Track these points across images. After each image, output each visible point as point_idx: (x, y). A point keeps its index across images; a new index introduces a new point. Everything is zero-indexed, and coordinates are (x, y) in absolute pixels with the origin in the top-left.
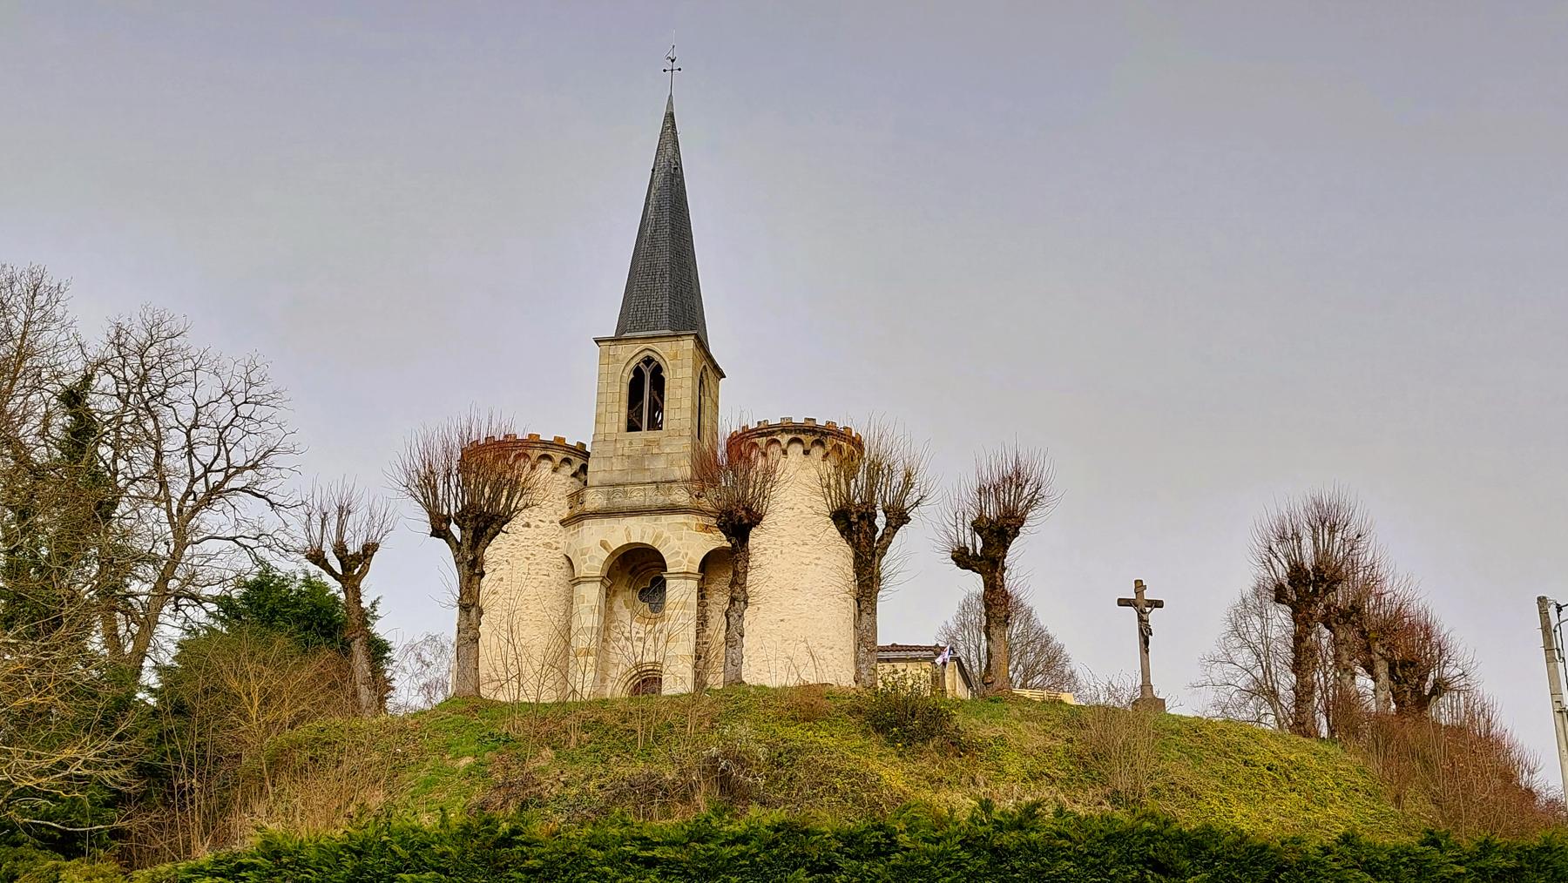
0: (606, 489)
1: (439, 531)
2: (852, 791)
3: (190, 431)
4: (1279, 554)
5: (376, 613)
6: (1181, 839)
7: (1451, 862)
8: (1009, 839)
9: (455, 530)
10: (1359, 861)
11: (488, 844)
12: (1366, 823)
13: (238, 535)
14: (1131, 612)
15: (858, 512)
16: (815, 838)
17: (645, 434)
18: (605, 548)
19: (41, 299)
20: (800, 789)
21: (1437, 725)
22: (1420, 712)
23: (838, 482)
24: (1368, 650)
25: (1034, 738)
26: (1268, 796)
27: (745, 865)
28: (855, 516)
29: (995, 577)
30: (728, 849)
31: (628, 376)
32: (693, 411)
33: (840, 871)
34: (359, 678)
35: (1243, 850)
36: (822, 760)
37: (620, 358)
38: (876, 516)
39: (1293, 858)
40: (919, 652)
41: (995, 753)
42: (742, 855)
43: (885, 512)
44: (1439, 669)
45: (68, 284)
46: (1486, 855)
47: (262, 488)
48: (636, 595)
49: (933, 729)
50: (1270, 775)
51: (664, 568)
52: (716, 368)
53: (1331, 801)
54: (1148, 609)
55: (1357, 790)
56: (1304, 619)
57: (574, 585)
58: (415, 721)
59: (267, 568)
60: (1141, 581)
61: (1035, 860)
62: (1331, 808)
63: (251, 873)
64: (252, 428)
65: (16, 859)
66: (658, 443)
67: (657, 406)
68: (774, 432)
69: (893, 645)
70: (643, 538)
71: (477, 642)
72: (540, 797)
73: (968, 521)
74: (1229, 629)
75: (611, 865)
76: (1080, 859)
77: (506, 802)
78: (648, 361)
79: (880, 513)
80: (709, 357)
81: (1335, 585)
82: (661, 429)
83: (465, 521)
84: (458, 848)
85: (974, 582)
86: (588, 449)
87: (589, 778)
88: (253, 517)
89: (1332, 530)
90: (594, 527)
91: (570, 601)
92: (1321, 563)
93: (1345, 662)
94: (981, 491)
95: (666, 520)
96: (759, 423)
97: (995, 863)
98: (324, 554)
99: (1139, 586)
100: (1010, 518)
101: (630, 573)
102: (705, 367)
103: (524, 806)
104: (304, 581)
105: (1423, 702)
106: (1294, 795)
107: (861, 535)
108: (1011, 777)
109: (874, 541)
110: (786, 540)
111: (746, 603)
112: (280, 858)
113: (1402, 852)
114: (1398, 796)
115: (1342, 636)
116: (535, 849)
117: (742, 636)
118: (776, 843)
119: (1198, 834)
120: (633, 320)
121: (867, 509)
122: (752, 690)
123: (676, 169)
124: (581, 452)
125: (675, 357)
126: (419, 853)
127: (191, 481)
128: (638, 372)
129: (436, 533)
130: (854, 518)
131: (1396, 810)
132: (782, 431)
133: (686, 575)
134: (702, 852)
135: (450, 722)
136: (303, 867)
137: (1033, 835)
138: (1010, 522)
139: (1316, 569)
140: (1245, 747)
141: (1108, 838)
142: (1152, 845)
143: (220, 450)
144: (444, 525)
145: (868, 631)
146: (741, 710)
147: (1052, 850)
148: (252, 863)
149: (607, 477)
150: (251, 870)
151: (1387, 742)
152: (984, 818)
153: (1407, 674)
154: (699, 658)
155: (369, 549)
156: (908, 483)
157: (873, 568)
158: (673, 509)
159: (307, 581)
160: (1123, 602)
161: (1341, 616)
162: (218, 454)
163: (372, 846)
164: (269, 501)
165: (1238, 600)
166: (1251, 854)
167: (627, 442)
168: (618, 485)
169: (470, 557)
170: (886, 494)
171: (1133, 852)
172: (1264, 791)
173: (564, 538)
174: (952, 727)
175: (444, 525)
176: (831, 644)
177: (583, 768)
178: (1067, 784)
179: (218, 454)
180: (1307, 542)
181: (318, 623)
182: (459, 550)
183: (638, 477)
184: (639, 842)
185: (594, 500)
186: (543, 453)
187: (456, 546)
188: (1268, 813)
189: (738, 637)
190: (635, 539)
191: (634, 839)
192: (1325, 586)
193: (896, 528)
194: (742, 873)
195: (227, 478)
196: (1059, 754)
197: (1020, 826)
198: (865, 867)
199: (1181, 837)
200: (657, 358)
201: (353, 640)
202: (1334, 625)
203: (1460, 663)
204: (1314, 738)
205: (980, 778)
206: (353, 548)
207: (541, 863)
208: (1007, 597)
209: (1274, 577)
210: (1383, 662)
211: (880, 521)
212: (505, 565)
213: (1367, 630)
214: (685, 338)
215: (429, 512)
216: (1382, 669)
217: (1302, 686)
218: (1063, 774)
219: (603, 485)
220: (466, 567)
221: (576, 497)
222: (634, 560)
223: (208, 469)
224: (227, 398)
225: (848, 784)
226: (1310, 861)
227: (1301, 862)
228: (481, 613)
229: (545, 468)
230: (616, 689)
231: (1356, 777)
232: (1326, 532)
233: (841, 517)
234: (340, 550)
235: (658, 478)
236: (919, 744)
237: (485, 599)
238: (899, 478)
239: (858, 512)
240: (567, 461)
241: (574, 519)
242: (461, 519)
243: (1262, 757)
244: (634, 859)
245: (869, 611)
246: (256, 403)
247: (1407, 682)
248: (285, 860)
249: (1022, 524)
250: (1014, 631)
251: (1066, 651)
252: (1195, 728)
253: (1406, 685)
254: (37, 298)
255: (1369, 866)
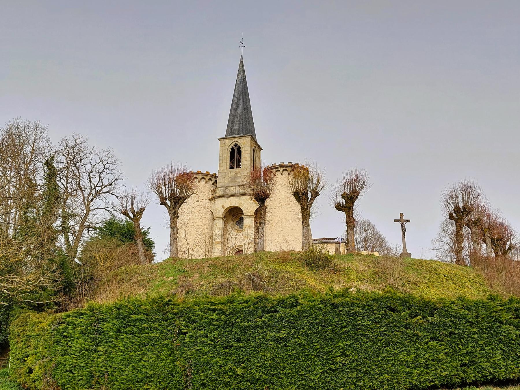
0: (223, 188)
1: (163, 203)
2: (296, 286)
3: (90, 174)
4: (450, 203)
5: (149, 232)
6: (400, 299)
7: (498, 306)
8: (338, 301)
9: (168, 202)
10: (464, 306)
11: (161, 305)
12: (479, 294)
13: (106, 207)
14: (399, 224)
15: (301, 192)
16: (269, 301)
17: (235, 170)
18: (223, 208)
19: (38, 132)
20: (279, 285)
21: (511, 261)
22: (504, 256)
23: (295, 183)
24: (484, 235)
25: (362, 267)
26: (444, 285)
27: (246, 311)
28: (301, 194)
29: (350, 213)
30: (240, 305)
31: (230, 150)
32: (251, 161)
33: (279, 312)
34: (140, 252)
35: (422, 303)
36: (287, 275)
37: (227, 145)
38: (308, 194)
39: (440, 305)
40: (332, 240)
41: (347, 272)
42: (245, 307)
43: (311, 192)
44: (511, 241)
45: (47, 127)
46: (511, 303)
47: (113, 192)
48: (235, 223)
49: (326, 264)
50: (445, 278)
51: (243, 214)
52: (259, 146)
53: (466, 287)
54: (405, 223)
55: (476, 283)
56: (459, 225)
57: (213, 220)
58: (156, 266)
59: (113, 216)
60: (402, 213)
61: (347, 308)
62: (466, 289)
63: (85, 316)
64: (109, 172)
65: (21, 313)
66: (239, 172)
67: (239, 161)
68: (278, 167)
69: (323, 238)
70: (235, 204)
71: (177, 239)
72: (193, 290)
73: (340, 194)
74: (441, 230)
75: (201, 311)
76: (363, 307)
77: (182, 292)
78: (236, 145)
79: (309, 193)
80: (256, 143)
81: (470, 213)
82: (241, 168)
83: (171, 199)
84: (151, 306)
85: (343, 215)
86: (217, 175)
87: (210, 283)
88: (111, 201)
89: (469, 194)
90: (220, 201)
91: (212, 225)
92: (465, 205)
93: (475, 239)
94: (345, 184)
95: (243, 198)
96: (273, 165)
97: (333, 309)
98: (127, 212)
99: (402, 215)
100: (354, 193)
101: (233, 216)
102: (255, 146)
103: (187, 293)
104: (125, 221)
105: (505, 253)
106: (453, 285)
107: (303, 200)
108: (352, 280)
109: (307, 202)
110: (283, 204)
111: (265, 224)
112: (93, 311)
113: (480, 303)
114: (491, 285)
115: (474, 230)
116: (176, 306)
117: (264, 235)
118: (257, 303)
119: (405, 298)
120: (231, 132)
121: (305, 191)
122: (266, 253)
123: (244, 80)
124: (215, 176)
125: (245, 143)
126: (138, 308)
127: (91, 190)
128: (233, 149)
129: (162, 204)
130: (300, 195)
131: (490, 289)
132: (281, 167)
133: (250, 216)
134: (232, 306)
135: (167, 266)
136: (101, 314)
137: (347, 299)
138: (355, 194)
139: (463, 207)
140: (437, 268)
141: (373, 300)
142: (389, 302)
143: (99, 179)
144: (164, 201)
145: (306, 233)
146: (261, 259)
147: (353, 304)
148: (85, 313)
149: (223, 184)
150: (85, 315)
151: (488, 266)
152: (331, 293)
153: (499, 243)
154: (256, 243)
155: (142, 210)
156: (318, 183)
157: (307, 211)
158: (245, 194)
159: (127, 221)
160: (396, 221)
161: (473, 223)
162: (99, 181)
163: (123, 306)
164: (116, 196)
165: (444, 220)
166: (425, 304)
167: (230, 172)
168: (227, 187)
169: (173, 211)
170: (311, 186)
171: (382, 304)
172: (442, 284)
173: (210, 205)
174: (333, 263)
175: (164, 201)
176: (299, 238)
177: (208, 280)
178: (372, 282)
179: (99, 181)
180: (460, 198)
181: (129, 235)
182: (170, 209)
183: (233, 184)
184: (210, 303)
185: (219, 192)
186: (202, 177)
187: (169, 208)
188: (443, 291)
189: (262, 235)
190: (237, 205)
191: (209, 302)
192: (466, 213)
193: (315, 198)
194: (245, 313)
195: (102, 188)
196: (370, 272)
197: (342, 296)
198: (287, 311)
199: (400, 299)
200: (239, 144)
201: (137, 240)
202: (471, 226)
203: (518, 239)
204: (463, 266)
205: (342, 281)
206: (137, 210)
207: (178, 311)
208: (354, 220)
209: (449, 211)
210: (489, 239)
211: (309, 195)
212: (191, 215)
213: (484, 228)
214: (248, 137)
215: (160, 197)
216: (489, 241)
217: (459, 248)
218: (371, 279)
219: (222, 187)
220: (172, 215)
221: (214, 191)
222: (233, 212)
223: (96, 186)
224: (101, 162)
225: (295, 283)
226: (446, 306)
227: (443, 307)
228: (178, 229)
229: (196, 181)
230: (229, 253)
231: (476, 278)
232: (467, 194)
233: (296, 194)
234: (132, 210)
235: (240, 184)
236: (321, 270)
237: (179, 225)
238: (315, 181)
239: (301, 192)
240: (210, 179)
241: (213, 199)
242: (170, 198)
243: (443, 272)
244: (209, 309)
245: (306, 226)
246: (110, 164)
247: (498, 246)
248: (95, 311)
249: (358, 195)
250: (369, 233)
251: (386, 240)
252: (420, 263)
253: (498, 247)
254: (37, 131)
255: (468, 308)
